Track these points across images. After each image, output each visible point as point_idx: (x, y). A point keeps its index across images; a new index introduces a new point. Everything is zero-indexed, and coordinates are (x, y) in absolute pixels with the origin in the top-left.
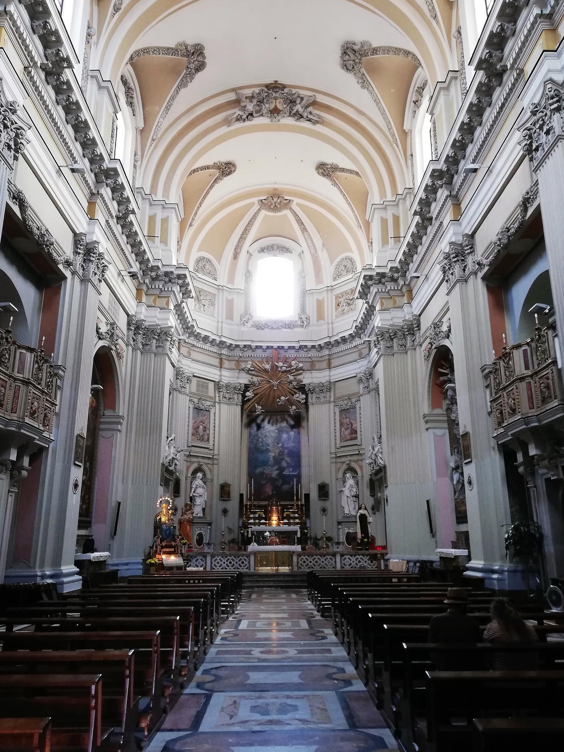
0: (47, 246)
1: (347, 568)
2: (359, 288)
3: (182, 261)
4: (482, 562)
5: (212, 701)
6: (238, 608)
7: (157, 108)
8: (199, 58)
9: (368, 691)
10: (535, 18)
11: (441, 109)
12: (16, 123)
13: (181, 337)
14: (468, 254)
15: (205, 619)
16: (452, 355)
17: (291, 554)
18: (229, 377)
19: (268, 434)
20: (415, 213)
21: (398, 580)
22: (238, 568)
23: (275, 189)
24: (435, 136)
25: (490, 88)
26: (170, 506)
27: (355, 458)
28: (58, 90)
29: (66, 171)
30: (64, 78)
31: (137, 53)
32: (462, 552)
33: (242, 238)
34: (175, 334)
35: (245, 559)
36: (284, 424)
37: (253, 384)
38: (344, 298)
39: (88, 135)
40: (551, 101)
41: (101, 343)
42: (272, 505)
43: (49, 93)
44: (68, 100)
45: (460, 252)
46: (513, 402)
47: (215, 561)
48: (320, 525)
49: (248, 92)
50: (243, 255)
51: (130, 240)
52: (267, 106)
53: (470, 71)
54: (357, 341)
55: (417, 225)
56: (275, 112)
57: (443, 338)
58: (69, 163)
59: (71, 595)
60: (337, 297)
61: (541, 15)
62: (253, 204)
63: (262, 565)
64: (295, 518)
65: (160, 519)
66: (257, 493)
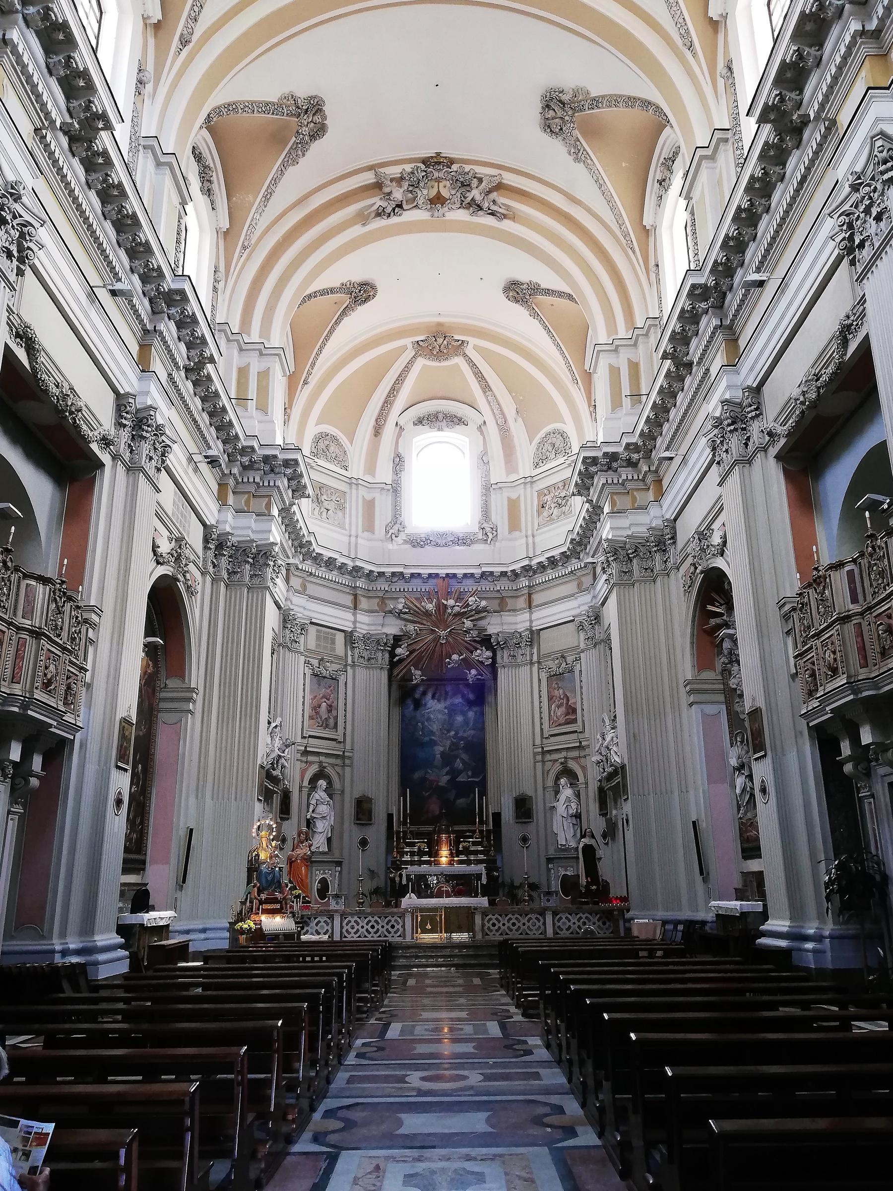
0: (71, 413)
1: (564, 933)
2: (576, 478)
3: (292, 440)
4: (788, 923)
5: (340, 1166)
6: (386, 1002)
7: (251, 197)
8: (316, 118)
9: (604, 1147)
10: (854, 37)
11: (703, 192)
12: (21, 216)
13: (291, 561)
14: (752, 418)
15: (327, 1022)
16: (730, 583)
17: (470, 912)
18: (369, 625)
19: (432, 716)
20: (665, 356)
21: (649, 953)
22: (386, 936)
23: (440, 324)
24: (694, 233)
25: (767, 185)
26: (274, 834)
27: (575, 754)
28: (89, 165)
29: (103, 295)
30: (98, 146)
31: (218, 110)
32: (756, 906)
33: (388, 403)
34: (280, 554)
35: (396, 921)
36: (458, 700)
37: (406, 635)
38: (552, 495)
39: (139, 236)
40: (882, 168)
41: (161, 570)
42: (440, 832)
43: (75, 170)
44: (105, 181)
45: (738, 417)
46: (832, 656)
47: (347, 924)
48: (520, 863)
49: (394, 171)
50: (389, 430)
51: (207, 405)
52: (425, 192)
53: (749, 126)
54: (574, 564)
55: (668, 374)
56: (438, 201)
57: (713, 555)
58: (108, 281)
59: (109, 984)
60: (540, 493)
61: (863, 33)
62: (405, 348)
63: (425, 931)
64: (476, 853)
65: (258, 855)
66: (417, 814)
